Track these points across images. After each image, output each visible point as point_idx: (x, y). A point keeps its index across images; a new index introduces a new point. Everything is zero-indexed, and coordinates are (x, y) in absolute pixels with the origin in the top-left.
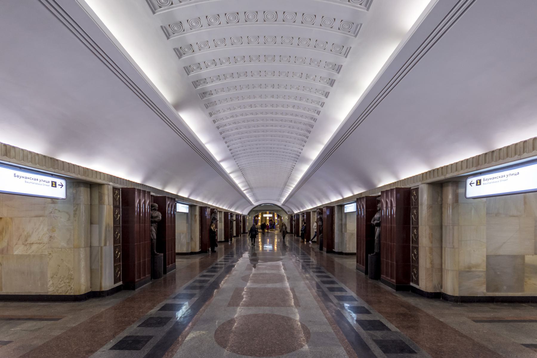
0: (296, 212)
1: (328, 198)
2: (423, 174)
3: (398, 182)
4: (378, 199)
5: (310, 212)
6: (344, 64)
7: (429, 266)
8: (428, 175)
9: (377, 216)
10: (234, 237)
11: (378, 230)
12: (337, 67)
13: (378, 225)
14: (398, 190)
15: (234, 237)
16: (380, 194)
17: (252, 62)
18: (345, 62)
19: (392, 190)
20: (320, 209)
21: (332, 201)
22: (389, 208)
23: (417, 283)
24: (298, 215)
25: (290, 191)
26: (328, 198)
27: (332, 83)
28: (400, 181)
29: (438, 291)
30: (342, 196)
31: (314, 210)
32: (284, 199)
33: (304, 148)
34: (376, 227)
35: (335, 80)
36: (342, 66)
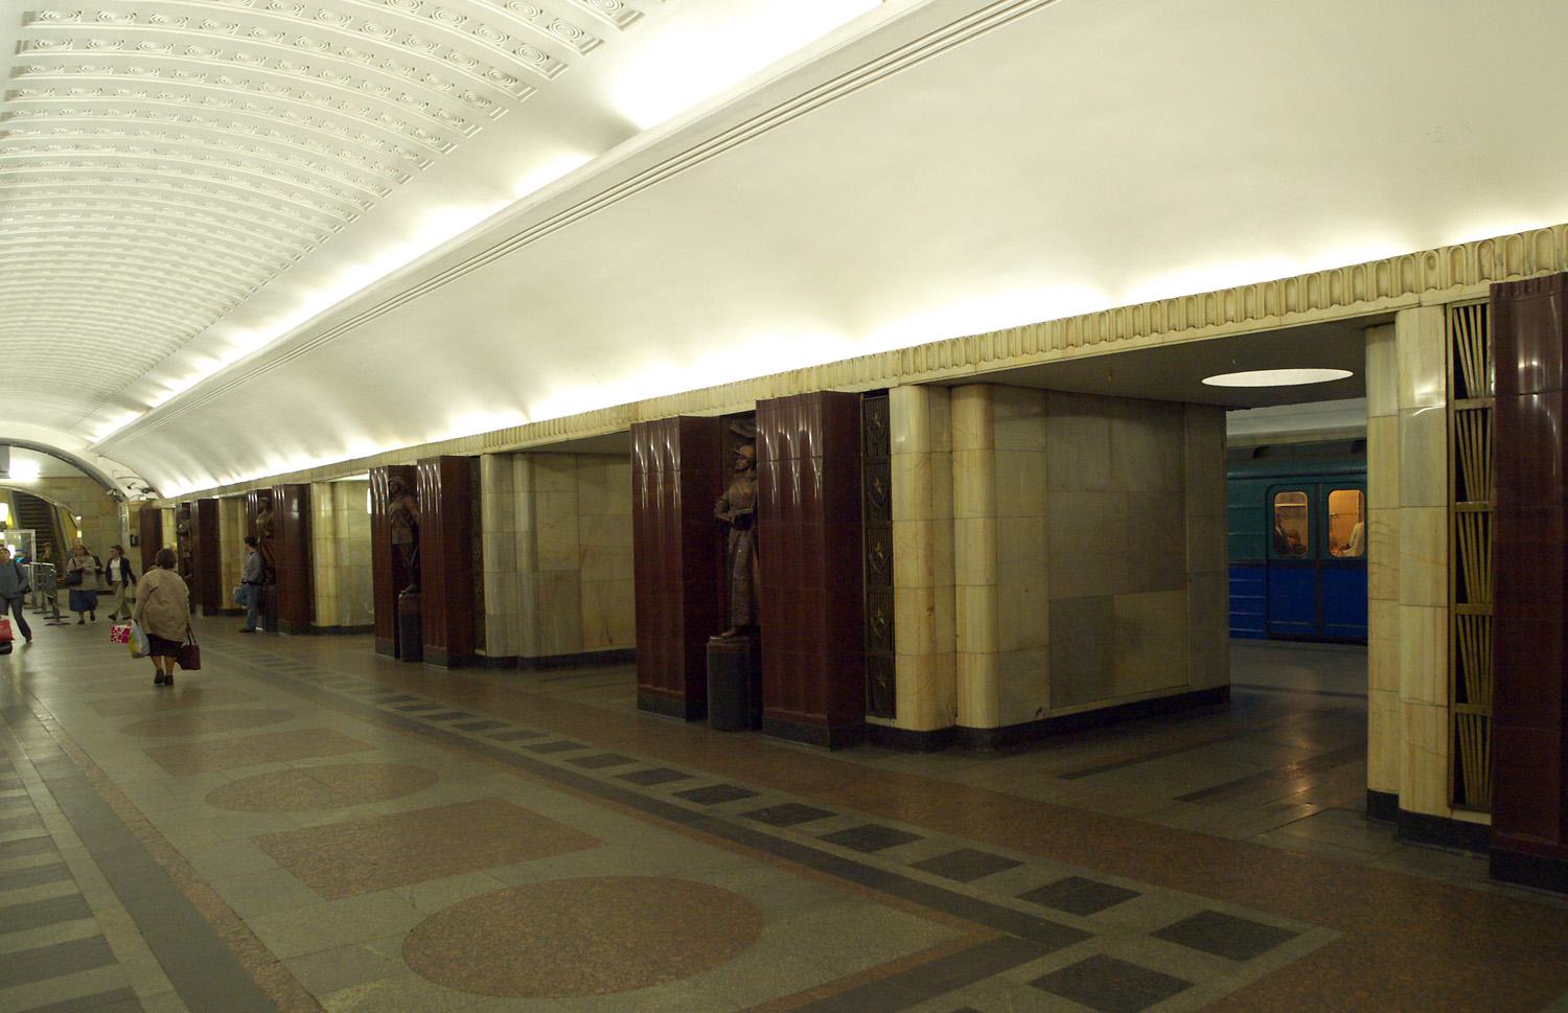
13: (745, 522)
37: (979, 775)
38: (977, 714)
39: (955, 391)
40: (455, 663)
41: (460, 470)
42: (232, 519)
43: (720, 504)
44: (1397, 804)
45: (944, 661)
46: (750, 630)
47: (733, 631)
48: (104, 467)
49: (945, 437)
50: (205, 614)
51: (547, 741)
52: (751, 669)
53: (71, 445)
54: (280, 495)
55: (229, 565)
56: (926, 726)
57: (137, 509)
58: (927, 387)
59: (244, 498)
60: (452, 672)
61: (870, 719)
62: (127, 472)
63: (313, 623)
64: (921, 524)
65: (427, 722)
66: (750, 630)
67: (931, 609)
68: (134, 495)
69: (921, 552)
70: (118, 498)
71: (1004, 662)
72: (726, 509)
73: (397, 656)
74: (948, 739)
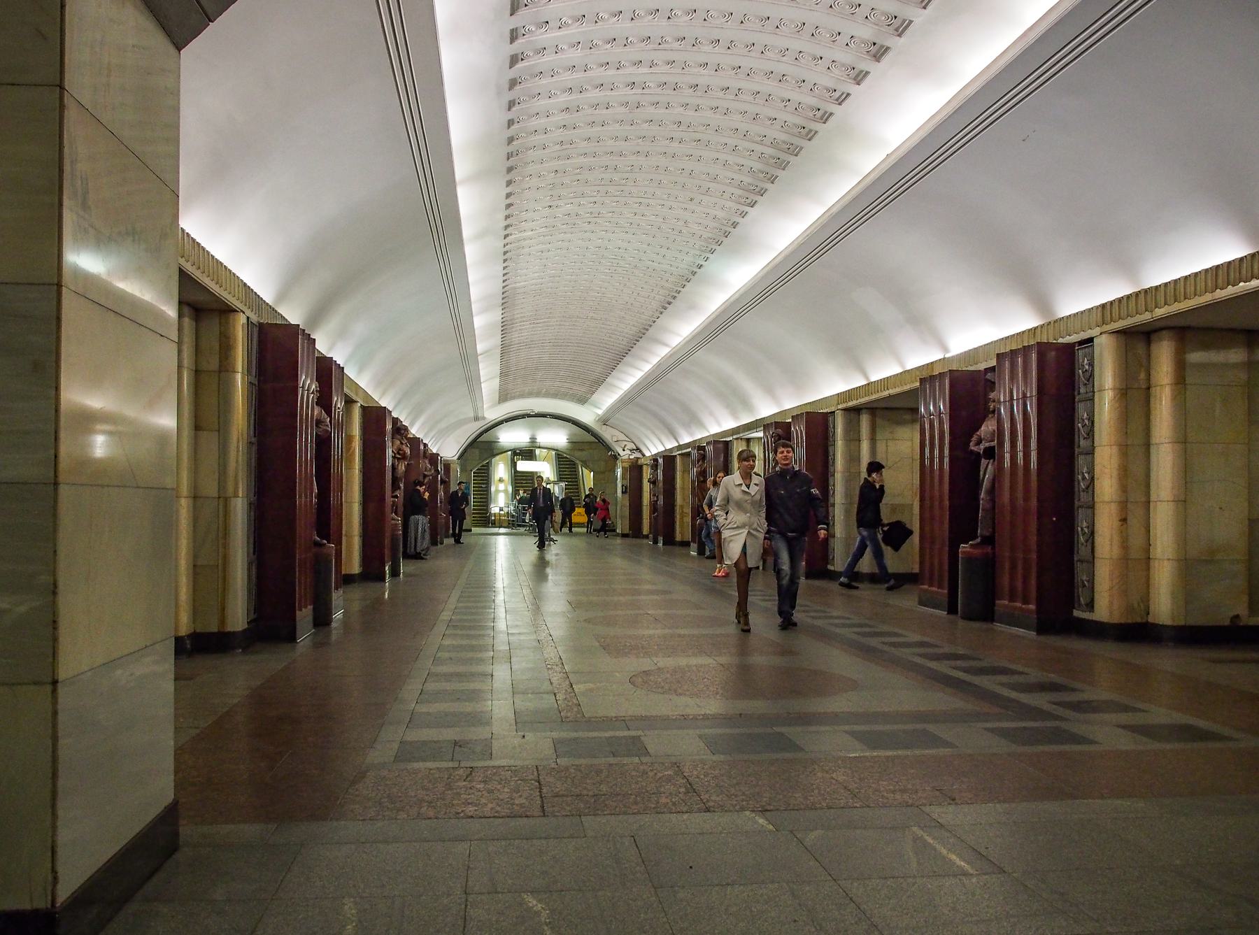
0: (655, 446)
1: (922, 324)
2: (1103, 306)
3: (1137, 294)
4: (989, 376)
5: (826, 416)
6: (917, 21)
7: (1116, 552)
8: (1132, 304)
9: (988, 427)
10: (348, 580)
11: (987, 471)
12: (897, 23)
13: (990, 453)
14: (1043, 348)
15: (348, 580)
16: (993, 363)
17: (600, 23)
18: (919, 17)
19: (1026, 350)
20: (701, 448)
21: (875, 377)
22: (1016, 402)
23: (1091, 606)
24: (668, 459)
25: (655, 360)
26: (922, 324)
27: (879, 52)
28: (1146, 291)
29: (1139, 620)
30: (867, 378)
31: (1009, 355)
32: (937, 612)
33: (752, 212)
34: (984, 462)
35: (888, 48)
36: (911, 22)
37: (1166, 661)
38: (1164, 606)
39: (1154, 337)
40: (1044, 626)
41: (816, 423)
42: (686, 471)
43: (974, 438)
44: (1224, 627)
45: (1137, 562)
46: (989, 540)
47: (979, 540)
48: (608, 434)
49: (1142, 376)
50: (807, 578)
51: (941, 651)
52: (987, 569)
53: (587, 415)
54: (710, 449)
55: (682, 507)
56: (1116, 618)
57: (626, 465)
58: (1124, 333)
59: (688, 454)
60: (1042, 638)
61: (1076, 613)
62: (622, 437)
63: (830, 567)
64: (1115, 450)
65: (886, 648)
66: (989, 540)
67: (1124, 520)
68: (625, 454)
69: (1115, 473)
70: (615, 457)
71: (1192, 567)
72: (979, 442)
73: (952, 610)
74: (1139, 632)
